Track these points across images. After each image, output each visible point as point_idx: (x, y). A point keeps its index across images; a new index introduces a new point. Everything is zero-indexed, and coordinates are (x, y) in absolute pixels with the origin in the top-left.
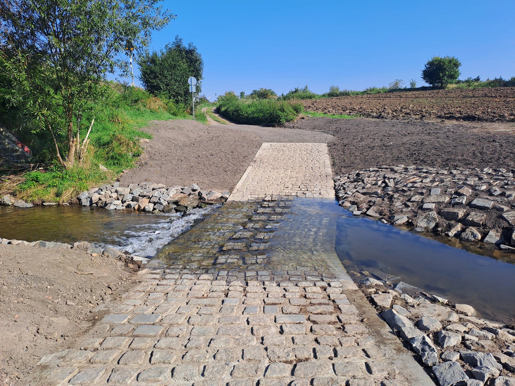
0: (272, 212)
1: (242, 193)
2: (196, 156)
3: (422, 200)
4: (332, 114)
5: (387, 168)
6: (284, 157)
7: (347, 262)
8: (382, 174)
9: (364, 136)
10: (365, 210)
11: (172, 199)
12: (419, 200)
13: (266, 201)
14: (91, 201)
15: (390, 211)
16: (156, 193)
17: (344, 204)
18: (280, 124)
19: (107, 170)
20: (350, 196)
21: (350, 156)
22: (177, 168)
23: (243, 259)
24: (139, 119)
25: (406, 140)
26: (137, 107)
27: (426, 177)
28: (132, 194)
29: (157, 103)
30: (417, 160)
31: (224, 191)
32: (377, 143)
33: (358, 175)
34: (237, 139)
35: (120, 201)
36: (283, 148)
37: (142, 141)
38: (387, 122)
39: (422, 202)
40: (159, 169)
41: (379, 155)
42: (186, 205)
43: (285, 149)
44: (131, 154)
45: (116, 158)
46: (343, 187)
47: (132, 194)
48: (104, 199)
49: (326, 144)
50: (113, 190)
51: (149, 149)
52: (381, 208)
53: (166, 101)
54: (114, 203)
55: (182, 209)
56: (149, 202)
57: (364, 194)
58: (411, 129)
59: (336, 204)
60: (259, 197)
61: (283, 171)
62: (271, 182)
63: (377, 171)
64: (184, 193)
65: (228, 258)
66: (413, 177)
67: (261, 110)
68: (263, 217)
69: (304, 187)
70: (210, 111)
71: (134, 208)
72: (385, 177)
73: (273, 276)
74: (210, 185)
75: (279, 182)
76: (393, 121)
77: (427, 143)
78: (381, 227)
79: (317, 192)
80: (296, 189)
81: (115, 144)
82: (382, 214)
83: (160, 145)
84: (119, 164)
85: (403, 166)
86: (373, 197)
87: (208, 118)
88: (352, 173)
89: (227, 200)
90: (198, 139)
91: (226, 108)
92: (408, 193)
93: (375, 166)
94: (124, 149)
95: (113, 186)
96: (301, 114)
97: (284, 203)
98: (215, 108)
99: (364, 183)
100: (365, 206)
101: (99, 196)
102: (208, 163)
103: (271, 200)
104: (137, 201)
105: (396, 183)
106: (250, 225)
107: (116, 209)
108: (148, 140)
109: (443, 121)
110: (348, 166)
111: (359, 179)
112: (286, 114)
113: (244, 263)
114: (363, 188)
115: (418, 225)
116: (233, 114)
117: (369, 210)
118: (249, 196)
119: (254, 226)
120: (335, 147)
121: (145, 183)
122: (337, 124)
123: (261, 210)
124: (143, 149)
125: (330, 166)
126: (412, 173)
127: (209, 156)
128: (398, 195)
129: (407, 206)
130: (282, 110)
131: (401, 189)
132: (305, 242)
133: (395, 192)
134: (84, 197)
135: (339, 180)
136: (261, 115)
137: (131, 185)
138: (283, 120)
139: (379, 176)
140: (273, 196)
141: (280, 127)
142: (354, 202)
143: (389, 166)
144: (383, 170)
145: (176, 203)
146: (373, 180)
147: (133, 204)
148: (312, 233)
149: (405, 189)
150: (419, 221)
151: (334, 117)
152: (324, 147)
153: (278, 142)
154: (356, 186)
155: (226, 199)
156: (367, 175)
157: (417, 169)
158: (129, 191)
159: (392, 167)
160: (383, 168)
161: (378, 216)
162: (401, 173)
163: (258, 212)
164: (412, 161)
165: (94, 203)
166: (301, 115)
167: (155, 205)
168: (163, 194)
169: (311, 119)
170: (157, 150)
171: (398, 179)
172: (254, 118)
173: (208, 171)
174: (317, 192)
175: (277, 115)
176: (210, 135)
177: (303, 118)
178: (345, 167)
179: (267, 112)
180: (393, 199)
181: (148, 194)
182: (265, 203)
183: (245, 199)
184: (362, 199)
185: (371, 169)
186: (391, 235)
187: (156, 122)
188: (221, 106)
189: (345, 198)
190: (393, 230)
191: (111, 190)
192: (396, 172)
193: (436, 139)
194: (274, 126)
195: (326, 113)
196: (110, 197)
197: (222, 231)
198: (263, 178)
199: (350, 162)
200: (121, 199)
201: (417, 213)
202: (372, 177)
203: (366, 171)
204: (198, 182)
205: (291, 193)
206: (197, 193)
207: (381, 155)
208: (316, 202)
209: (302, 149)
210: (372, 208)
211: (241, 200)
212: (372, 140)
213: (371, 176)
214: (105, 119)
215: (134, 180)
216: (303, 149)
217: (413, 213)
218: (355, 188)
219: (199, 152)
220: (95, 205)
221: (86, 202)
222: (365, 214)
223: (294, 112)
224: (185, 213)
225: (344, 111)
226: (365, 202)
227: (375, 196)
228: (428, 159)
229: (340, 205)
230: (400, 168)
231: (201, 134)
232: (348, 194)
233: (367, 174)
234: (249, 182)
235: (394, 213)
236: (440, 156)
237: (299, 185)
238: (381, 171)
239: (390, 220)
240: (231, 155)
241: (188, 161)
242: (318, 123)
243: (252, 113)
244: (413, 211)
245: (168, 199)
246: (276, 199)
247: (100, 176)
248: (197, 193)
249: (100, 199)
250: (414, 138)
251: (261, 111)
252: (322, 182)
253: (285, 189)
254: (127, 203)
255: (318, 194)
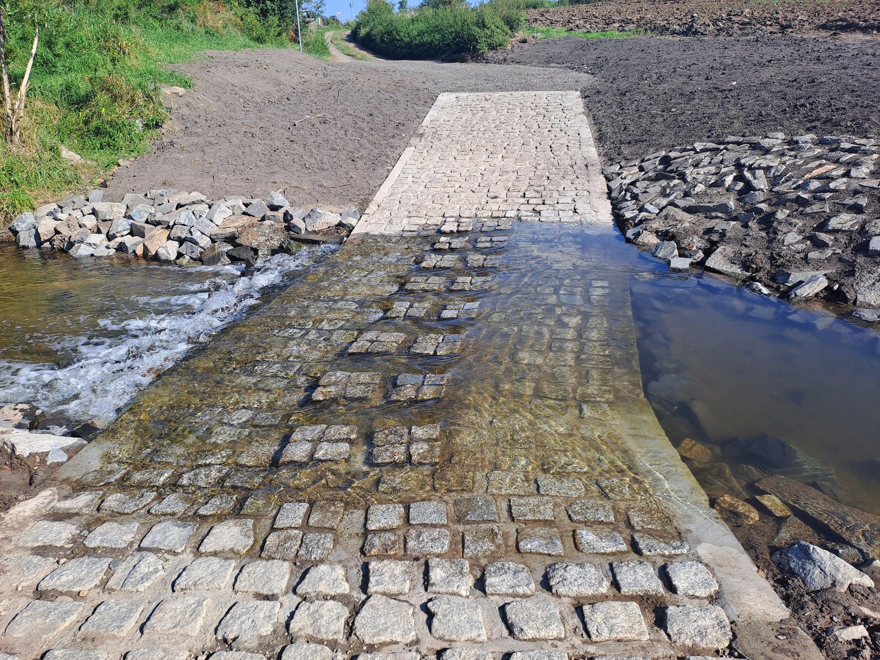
0: (460, 265)
1: (388, 213)
2: (288, 124)
3: (863, 227)
4: (585, 30)
5: (739, 143)
6: (485, 123)
7: (699, 450)
8: (730, 156)
9: (664, 70)
10: (701, 255)
11: (220, 232)
12: (852, 226)
13: (444, 234)
14: (37, 236)
15: (772, 258)
16: (183, 216)
17: (640, 239)
18: (477, 56)
19: (83, 161)
20: (654, 216)
21: (640, 117)
22: (240, 154)
23: (368, 438)
24: (177, 48)
25: (768, 75)
26: (175, 22)
27: (856, 164)
28: (130, 217)
29: (219, 16)
30: (813, 121)
31: (345, 209)
32: (699, 84)
33: (666, 161)
34: (384, 86)
35: (103, 236)
36: (484, 104)
37: (168, 92)
38: (708, 40)
39: (862, 231)
40: (198, 156)
41: (709, 111)
42: (254, 245)
43: (487, 105)
44: (139, 123)
45: (106, 133)
46: (632, 193)
47: (130, 217)
48: (65, 231)
49: (578, 93)
50: (87, 210)
51: (185, 111)
52: (745, 251)
53: (241, 11)
54: (88, 241)
55: (244, 255)
56: (169, 238)
57: (689, 210)
58: (768, 52)
59: (617, 237)
60: (429, 222)
61: (485, 157)
62: (457, 186)
63: (716, 151)
64: (249, 215)
65: (320, 440)
66: (818, 163)
67: (436, 27)
68: (436, 282)
69: (534, 194)
70: (339, 37)
71: (134, 251)
72: (739, 166)
73: (461, 528)
74: (315, 193)
75: (477, 184)
76: (721, 38)
77: (824, 80)
78: (756, 306)
79: (567, 207)
80: (516, 200)
81: (103, 97)
82: (750, 267)
83: (211, 102)
84: (111, 146)
85: (781, 135)
86: (717, 217)
87: (332, 49)
88: (651, 156)
89: (351, 231)
90: (300, 88)
91: (367, 29)
92: (816, 208)
93: (704, 138)
94: (122, 110)
95: (88, 200)
96: (521, 32)
97: (489, 239)
98: (349, 32)
99: (685, 181)
100: (697, 243)
101: (55, 223)
102: (312, 140)
103: (458, 231)
104: (143, 236)
105: (774, 181)
106: (400, 307)
107: (92, 255)
108: (181, 90)
109: (835, 34)
110: (637, 142)
111: (671, 171)
112: (488, 32)
113: (370, 461)
114: (687, 194)
115: (860, 298)
116: (382, 41)
117: (713, 256)
118: (405, 221)
119: (412, 312)
120: (601, 97)
121: (160, 191)
122: (598, 51)
123: (431, 260)
124: (169, 110)
125: (592, 142)
126: (811, 154)
127: (318, 125)
128: (788, 212)
129: (820, 245)
130: (482, 25)
131: (792, 196)
132: (553, 367)
133: (777, 205)
134: (24, 226)
135: (619, 174)
136: (437, 36)
137: (129, 197)
138: (483, 47)
139: (722, 162)
140: (462, 220)
141: (477, 61)
142: (667, 232)
143: (743, 136)
144: (730, 146)
145: (231, 239)
146: (708, 173)
147: (129, 241)
148: (570, 334)
149: (805, 196)
150: (862, 287)
151: (589, 36)
152: (574, 100)
153: (472, 91)
154: (664, 188)
155: (351, 229)
156: (690, 161)
157: (821, 142)
158: (123, 210)
159: (755, 139)
160: (728, 143)
161: (739, 271)
162: (783, 155)
163: (424, 264)
164: (800, 122)
165: (46, 241)
166: (520, 34)
167: (181, 245)
168: (200, 216)
169: (541, 42)
170: (202, 113)
171: (777, 170)
172: (423, 44)
173: (312, 160)
174: (567, 207)
175: (470, 35)
176: (326, 80)
177: (525, 41)
178: (629, 143)
179: (450, 30)
180: (775, 224)
181: (165, 218)
182: (443, 239)
183: (394, 230)
184: (688, 225)
185: (699, 146)
186: (790, 333)
187: (214, 52)
188: (359, 25)
189: (641, 222)
190: (790, 317)
191: (84, 209)
192: (767, 151)
193: (843, 71)
194: (463, 61)
195: (571, 29)
196: (80, 226)
197: (326, 327)
198: (439, 175)
199: (640, 130)
200: (104, 230)
201: (852, 264)
202: (704, 166)
203: (685, 150)
204: (287, 186)
205: (506, 211)
206: (280, 214)
207: (715, 110)
208: (569, 234)
209: (525, 104)
210: (719, 250)
211: (386, 233)
212: (684, 79)
213: (702, 164)
214: (89, 44)
215: (139, 185)
216: (529, 104)
217: (839, 265)
218: (664, 194)
219: (296, 116)
220: (47, 245)
221: (26, 239)
222: (701, 264)
223: (506, 28)
224: (249, 265)
225: (607, 24)
226: (695, 233)
227: (720, 215)
228: (843, 117)
229: (628, 240)
230: (776, 139)
231: (307, 77)
232: (647, 211)
233: (691, 158)
234: (406, 187)
235: (783, 265)
236: (875, 109)
237: (523, 189)
238: (725, 148)
239: (775, 285)
240: (368, 123)
241: (269, 137)
242: (557, 50)
243: (419, 35)
244: (841, 260)
245: (212, 230)
246: (470, 229)
247: (62, 175)
248: (280, 214)
249: (57, 232)
250: (786, 70)
251: (437, 29)
252: (577, 182)
253: (490, 200)
254: (119, 240)
255: (571, 213)
